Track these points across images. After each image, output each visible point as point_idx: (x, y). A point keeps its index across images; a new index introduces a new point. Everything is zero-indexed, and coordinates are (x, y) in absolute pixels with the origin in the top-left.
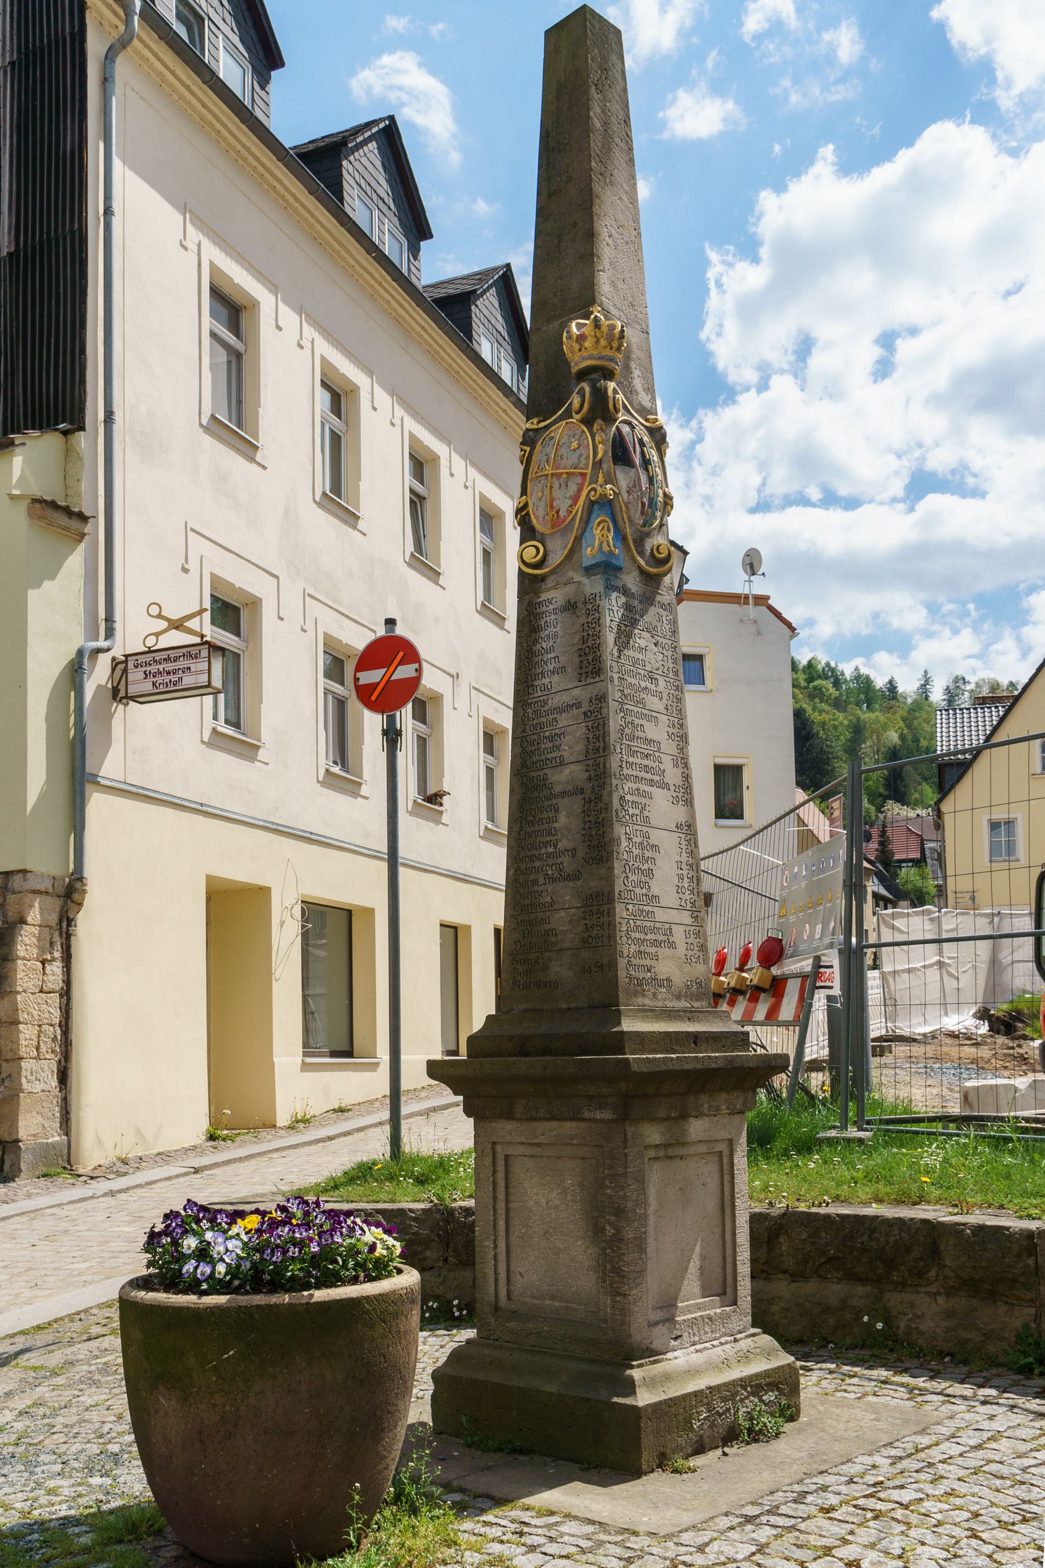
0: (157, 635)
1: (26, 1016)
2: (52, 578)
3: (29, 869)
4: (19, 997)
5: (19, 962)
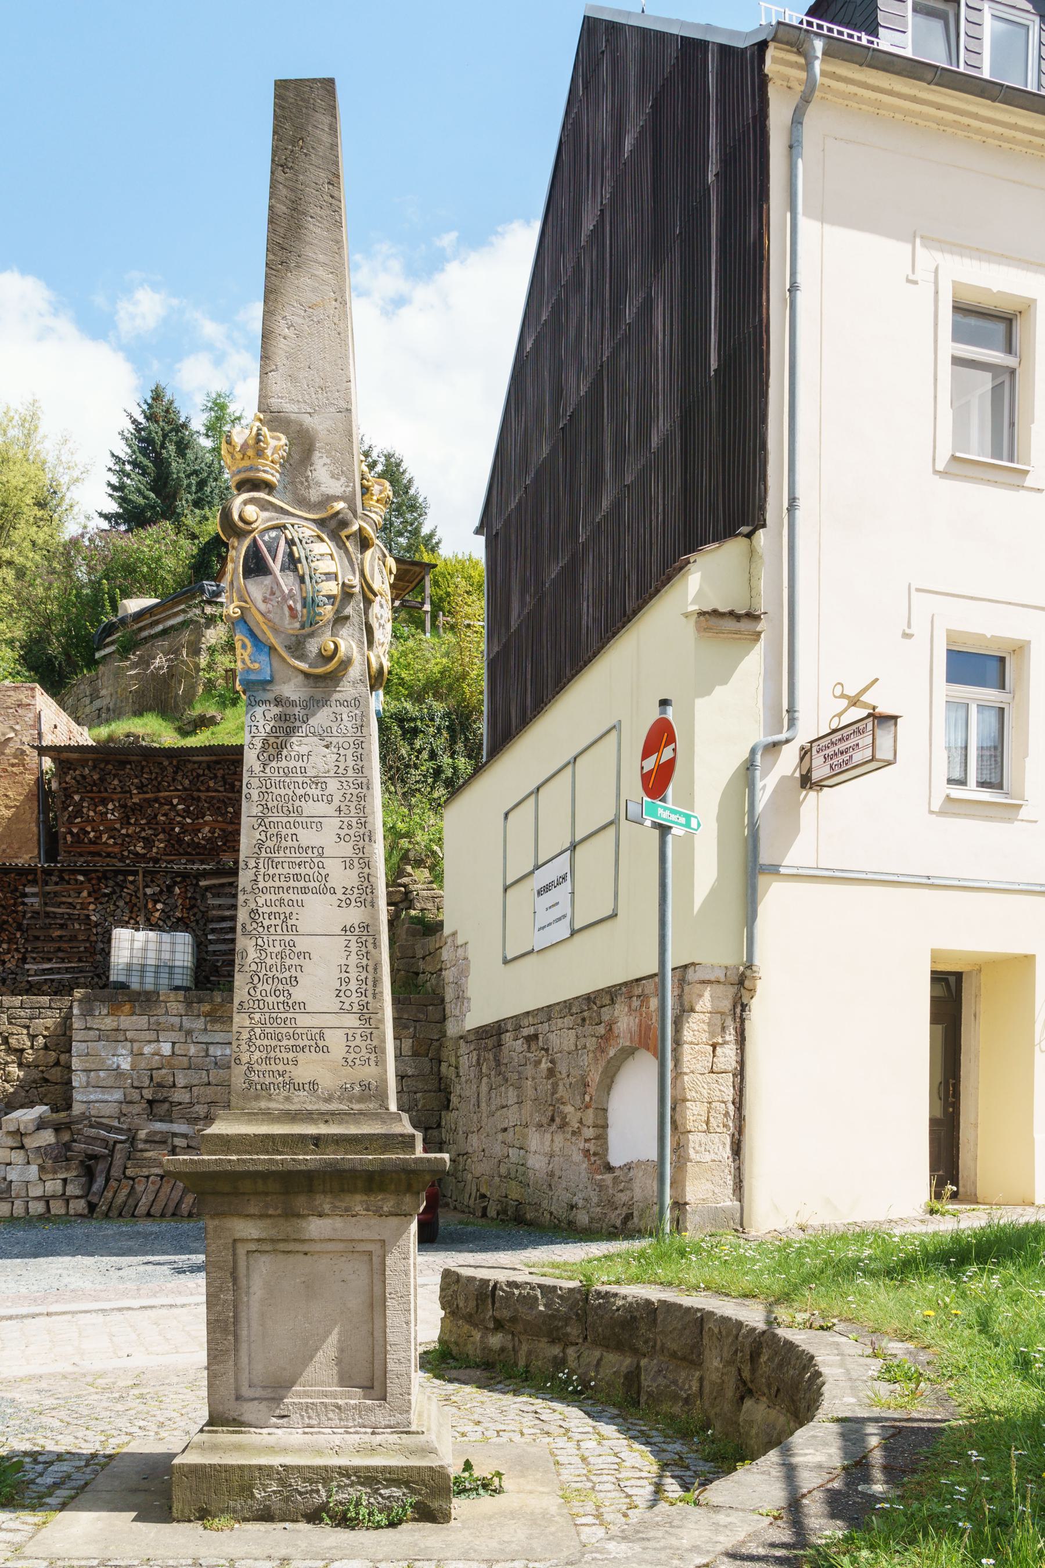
0: (839, 715)
1: (694, 1094)
2: (724, 680)
3: (696, 961)
4: (686, 1078)
5: (686, 1046)
